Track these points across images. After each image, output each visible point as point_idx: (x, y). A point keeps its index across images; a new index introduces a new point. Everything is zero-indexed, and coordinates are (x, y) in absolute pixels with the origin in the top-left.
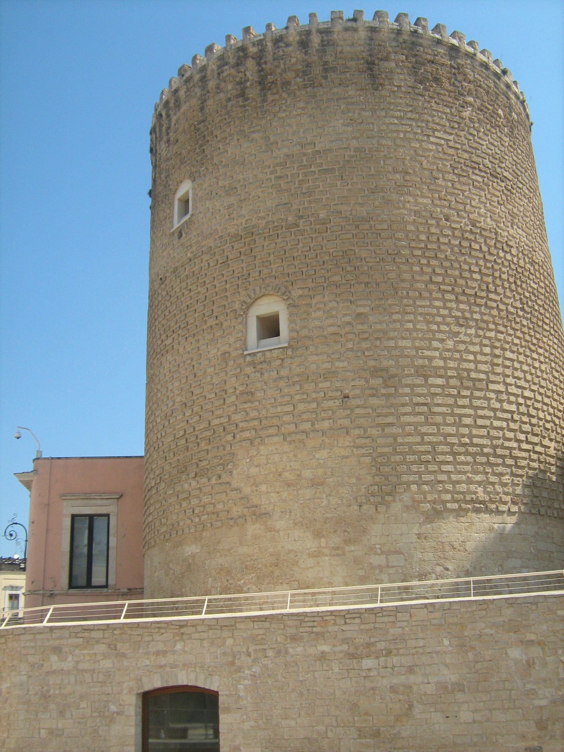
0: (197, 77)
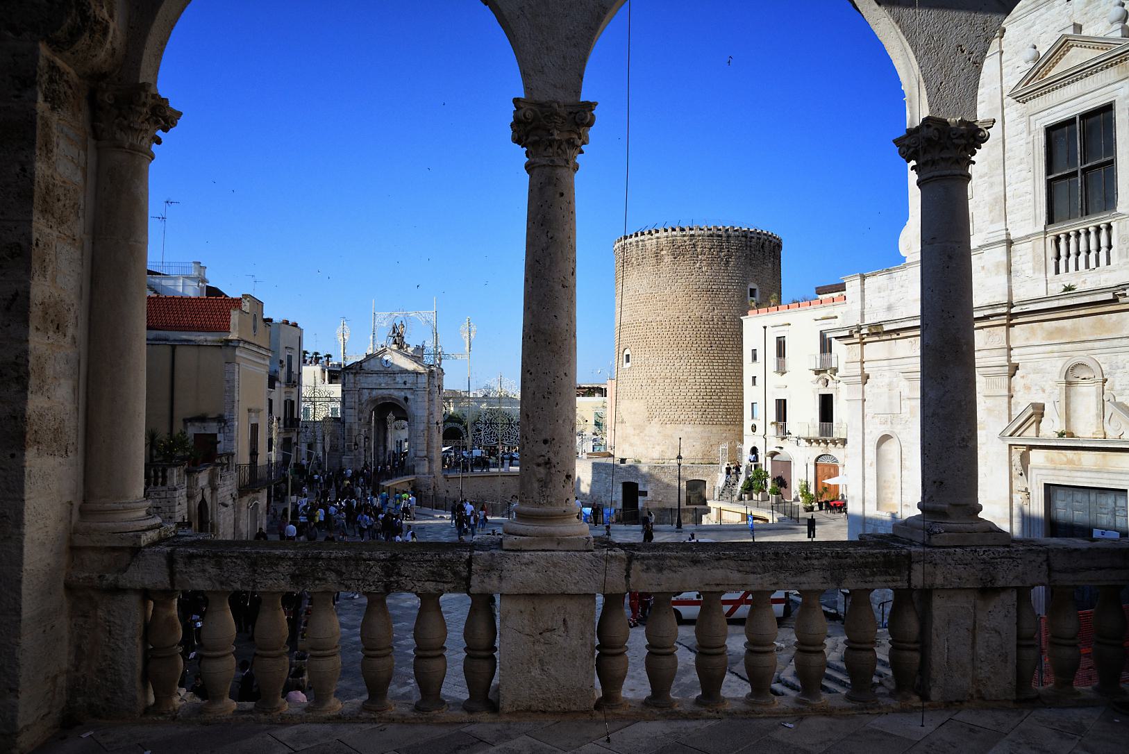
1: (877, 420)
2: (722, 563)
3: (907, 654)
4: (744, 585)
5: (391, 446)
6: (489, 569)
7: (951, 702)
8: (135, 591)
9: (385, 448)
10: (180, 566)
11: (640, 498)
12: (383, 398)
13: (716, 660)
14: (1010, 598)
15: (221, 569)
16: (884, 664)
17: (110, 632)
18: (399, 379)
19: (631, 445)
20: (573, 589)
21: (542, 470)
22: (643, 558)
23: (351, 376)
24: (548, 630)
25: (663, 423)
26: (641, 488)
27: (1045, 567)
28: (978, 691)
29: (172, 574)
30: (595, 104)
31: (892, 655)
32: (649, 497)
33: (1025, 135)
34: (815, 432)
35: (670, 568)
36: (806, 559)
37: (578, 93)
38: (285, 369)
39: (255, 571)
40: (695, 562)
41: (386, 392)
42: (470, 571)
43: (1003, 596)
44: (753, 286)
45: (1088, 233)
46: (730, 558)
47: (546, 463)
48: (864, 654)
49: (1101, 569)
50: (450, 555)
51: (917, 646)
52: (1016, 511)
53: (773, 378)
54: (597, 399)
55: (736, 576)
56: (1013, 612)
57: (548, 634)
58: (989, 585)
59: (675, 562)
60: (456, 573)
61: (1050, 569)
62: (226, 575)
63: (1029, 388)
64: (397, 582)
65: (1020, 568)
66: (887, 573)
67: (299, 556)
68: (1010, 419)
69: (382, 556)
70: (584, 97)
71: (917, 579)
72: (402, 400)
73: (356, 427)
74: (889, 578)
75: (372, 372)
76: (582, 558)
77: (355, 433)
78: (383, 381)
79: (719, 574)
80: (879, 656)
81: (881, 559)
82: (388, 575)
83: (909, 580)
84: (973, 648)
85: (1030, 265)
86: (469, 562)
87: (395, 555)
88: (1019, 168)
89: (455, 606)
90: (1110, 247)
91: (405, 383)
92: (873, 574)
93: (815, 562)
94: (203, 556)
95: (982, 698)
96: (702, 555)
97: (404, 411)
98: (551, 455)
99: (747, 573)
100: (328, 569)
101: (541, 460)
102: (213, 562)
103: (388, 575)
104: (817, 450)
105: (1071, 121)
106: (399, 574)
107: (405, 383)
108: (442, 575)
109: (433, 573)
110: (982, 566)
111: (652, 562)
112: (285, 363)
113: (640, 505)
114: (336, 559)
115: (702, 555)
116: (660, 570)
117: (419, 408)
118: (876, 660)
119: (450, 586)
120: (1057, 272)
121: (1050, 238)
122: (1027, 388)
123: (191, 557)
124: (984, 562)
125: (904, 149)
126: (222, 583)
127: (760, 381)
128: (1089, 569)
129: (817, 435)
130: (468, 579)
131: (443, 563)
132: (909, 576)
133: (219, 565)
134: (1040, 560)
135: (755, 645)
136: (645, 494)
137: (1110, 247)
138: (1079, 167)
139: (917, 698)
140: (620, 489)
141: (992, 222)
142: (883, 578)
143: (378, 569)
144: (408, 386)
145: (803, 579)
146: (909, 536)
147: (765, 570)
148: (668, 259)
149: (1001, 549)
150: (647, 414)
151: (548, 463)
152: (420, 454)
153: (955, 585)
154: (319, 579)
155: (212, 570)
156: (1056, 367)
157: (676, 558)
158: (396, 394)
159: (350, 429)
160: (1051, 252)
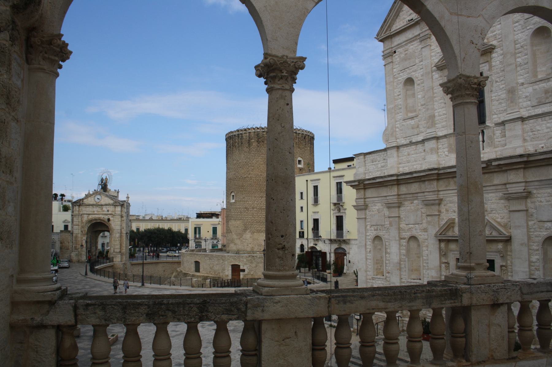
1: (372, 228)
2: (375, 297)
3: (459, 339)
4: (385, 309)
5: (100, 247)
6: (256, 306)
7: (480, 362)
8: (53, 326)
9: (96, 247)
10: (81, 311)
11: (241, 273)
12: (95, 219)
13: (371, 349)
14: (505, 308)
15: (105, 312)
16: (380, 354)
17: (37, 352)
18: (105, 209)
19: (235, 244)
20: (302, 315)
21: (281, 252)
22: (337, 297)
23: (77, 207)
24: (288, 338)
25: (253, 233)
26: (241, 268)
27: (519, 292)
28: (492, 356)
29: (76, 315)
30: (306, 58)
31: (385, 349)
32: (246, 272)
34: (334, 237)
35: (349, 301)
36: (415, 293)
37: (295, 52)
39: (125, 312)
40: (362, 298)
41: (97, 216)
42: (246, 308)
43: (502, 307)
44: (299, 159)
46: (379, 295)
47: (283, 248)
48: (438, 341)
49: (542, 292)
50: (235, 299)
51: (464, 335)
53: (312, 209)
55: (381, 305)
56: (506, 315)
57: (287, 340)
58: (496, 302)
59: (352, 298)
60: (238, 309)
61: (522, 293)
62: (108, 315)
63: (448, 211)
64: (206, 316)
65: (509, 294)
66: (452, 299)
67: (151, 303)
69: (198, 302)
70: (299, 54)
71: (466, 301)
72: (106, 220)
73: (79, 235)
74: (452, 301)
75: (89, 205)
76: (305, 298)
77: (79, 239)
78: (96, 210)
79: (374, 303)
80: (377, 350)
81: (449, 292)
82: (201, 312)
83: (461, 301)
84: (489, 334)
85: (447, 149)
86: (246, 304)
87: (205, 301)
88: (440, 101)
89: (235, 327)
91: (108, 211)
92: (445, 300)
93: (419, 295)
94: (94, 305)
95: (493, 359)
96: (366, 294)
97: (107, 227)
98: (285, 243)
99: (387, 302)
100: (168, 310)
101: (280, 246)
102: (101, 307)
103: (201, 312)
104: (335, 246)
106: (207, 311)
107: (108, 211)
108: (232, 311)
109: (226, 309)
110: (493, 293)
111: (341, 299)
113: (241, 277)
114: (172, 304)
115: (366, 294)
116: (345, 303)
117: (116, 224)
118: (376, 352)
119: (235, 316)
123: (88, 305)
124: (494, 291)
125: (445, 89)
126: (105, 320)
127: (305, 209)
128: (537, 292)
129: (335, 238)
130: (245, 313)
131: (232, 304)
132: (461, 300)
133: (104, 309)
134: (517, 289)
135: (411, 338)
137: (483, 141)
139: (464, 361)
140: (230, 268)
141: (428, 128)
142: (449, 302)
143: (195, 309)
144: (110, 212)
145: (413, 304)
146: (456, 281)
147: (396, 300)
148: (255, 144)
149: (500, 285)
150: (243, 228)
151: (283, 248)
152: (116, 250)
153: (481, 304)
154: (163, 316)
155: (100, 313)
157: (353, 296)
158: (102, 216)
159: (76, 237)
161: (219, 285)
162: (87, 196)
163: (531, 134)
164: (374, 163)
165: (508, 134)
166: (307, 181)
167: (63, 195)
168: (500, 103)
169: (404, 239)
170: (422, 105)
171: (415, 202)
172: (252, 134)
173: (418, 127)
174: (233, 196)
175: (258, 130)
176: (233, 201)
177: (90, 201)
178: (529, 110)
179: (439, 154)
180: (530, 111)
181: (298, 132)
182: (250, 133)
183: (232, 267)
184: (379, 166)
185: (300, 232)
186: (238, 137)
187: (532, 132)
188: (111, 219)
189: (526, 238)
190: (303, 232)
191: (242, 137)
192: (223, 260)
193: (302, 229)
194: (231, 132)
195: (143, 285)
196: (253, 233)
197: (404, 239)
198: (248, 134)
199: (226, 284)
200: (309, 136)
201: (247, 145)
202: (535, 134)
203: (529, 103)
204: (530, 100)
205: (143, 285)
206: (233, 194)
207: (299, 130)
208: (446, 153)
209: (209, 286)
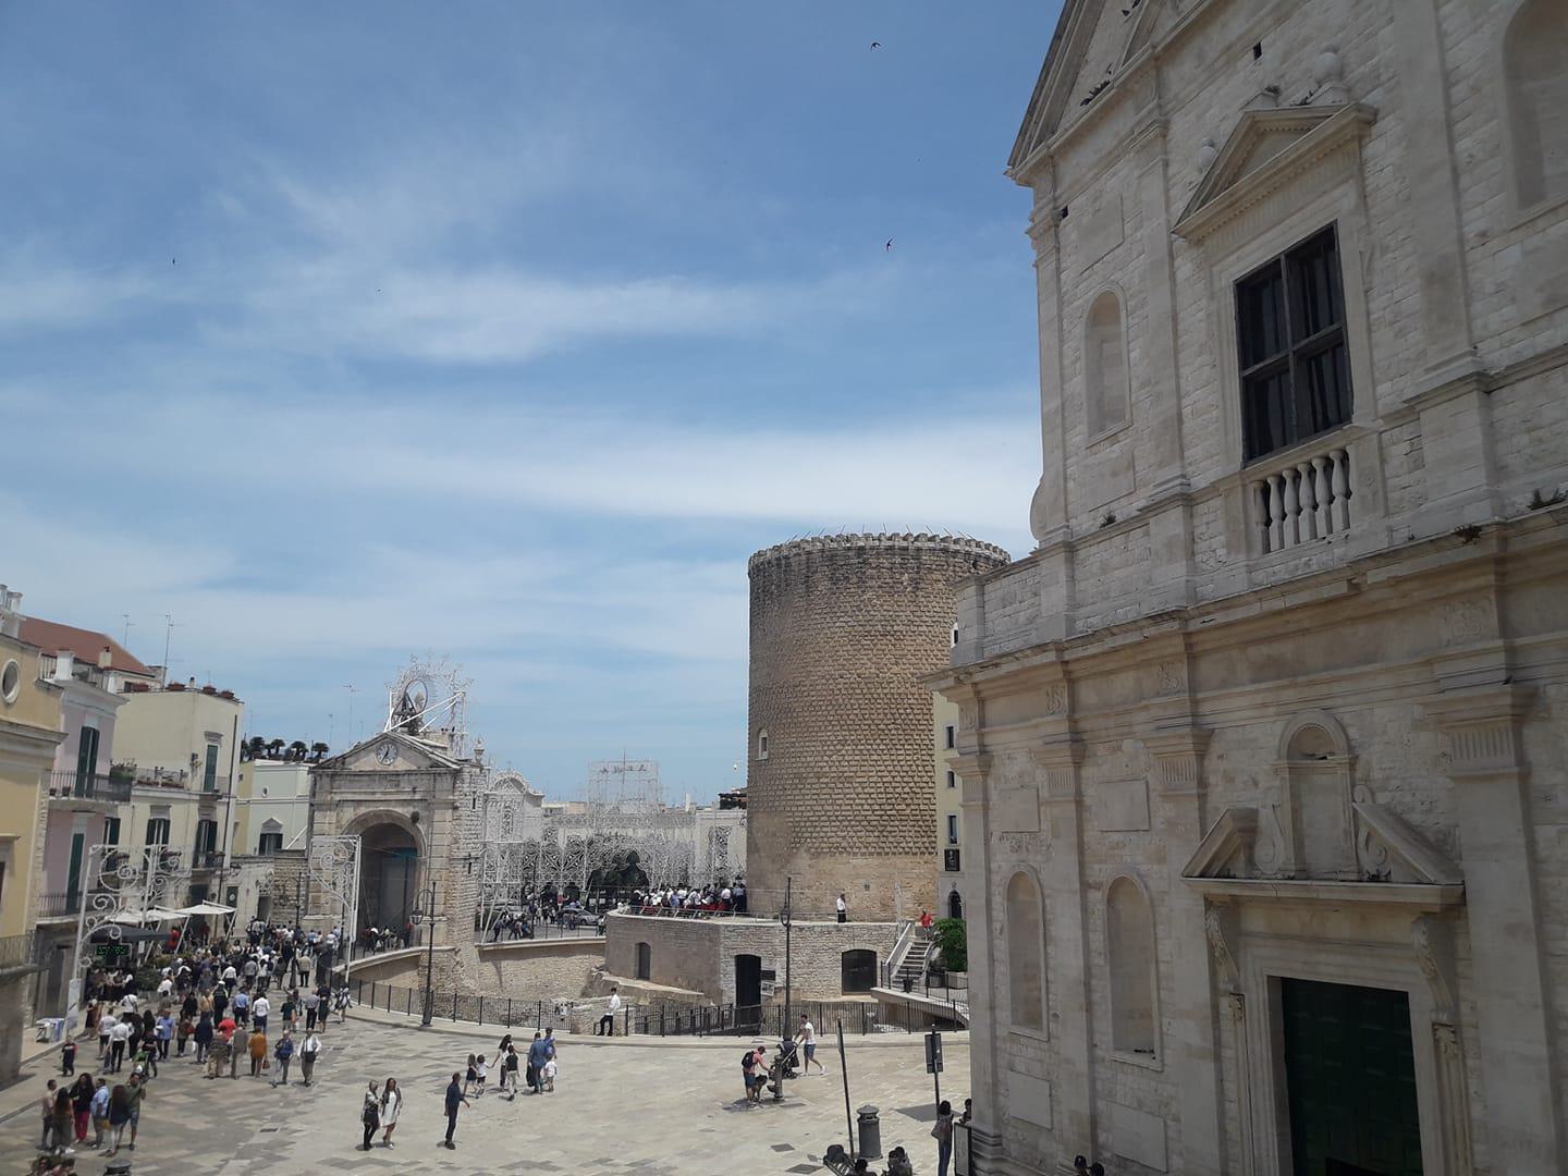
0: (775, 562)
26: (764, 966)
33: (1204, 302)
38: (202, 771)
45: (1312, 472)
52: (855, 1117)
54: (471, 806)
68: (1203, 833)
85: (1222, 538)
90: (1348, 494)
105: (1274, 265)
112: (202, 758)
120: (1267, 549)
121: (1253, 488)
122: (1229, 779)
136: (771, 975)
137: (1348, 494)
138: (1290, 349)
140: (732, 969)
141: (1161, 465)
148: (824, 586)
156: (1270, 734)
160: (1256, 514)
161: (670, 1023)
162: (359, 750)
163: (1525, 439)
164: (1008, 610)
165: (1430, 451)
166: (449, 1144)
167: (321, 748)
168: (1401, 333)
169: (1098, 887)
170: (1143, 385)
171: (1127, 744)
172: (816, 557)
173: (1132, 466)
174: (765, 739)
175: (835, 545)
176: (765, 755)
177: (369, 762)
178: (1512, 342)
179: (1198, 558)
180: (1515, 347)
181: (953, 547)
182: (809, 553)
183: (737, 965)
184: (1022, 617)
185: (947, 852)
186: (779, 565)
187: (1529, 431)
188: (423, 814)
189: (1526, 904)
190: (957, 852)
191: (788, 565)
192: (711, 940)
193: (954, 841)
194: (759, 554)
195: (426, 1023)
196: (817, 855)
197: (1098, 887)
198: (804, 557)
199: (714, 1020)
200: (988, 558)
201: (801, 589)
202: (1540, 440)
203: (1509, 311)
204: (1513, 300)
205: (426, 1023)
206: (764, 734)
207: (956, 542)
208: (1221, 552)
209: (623, 1031)
